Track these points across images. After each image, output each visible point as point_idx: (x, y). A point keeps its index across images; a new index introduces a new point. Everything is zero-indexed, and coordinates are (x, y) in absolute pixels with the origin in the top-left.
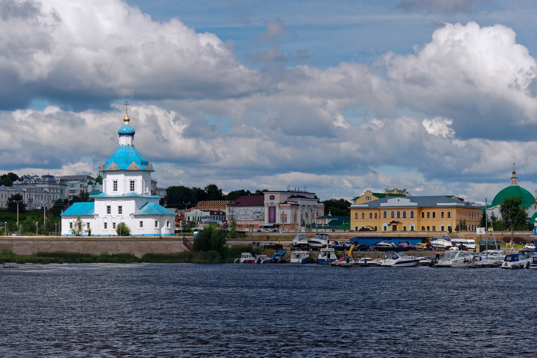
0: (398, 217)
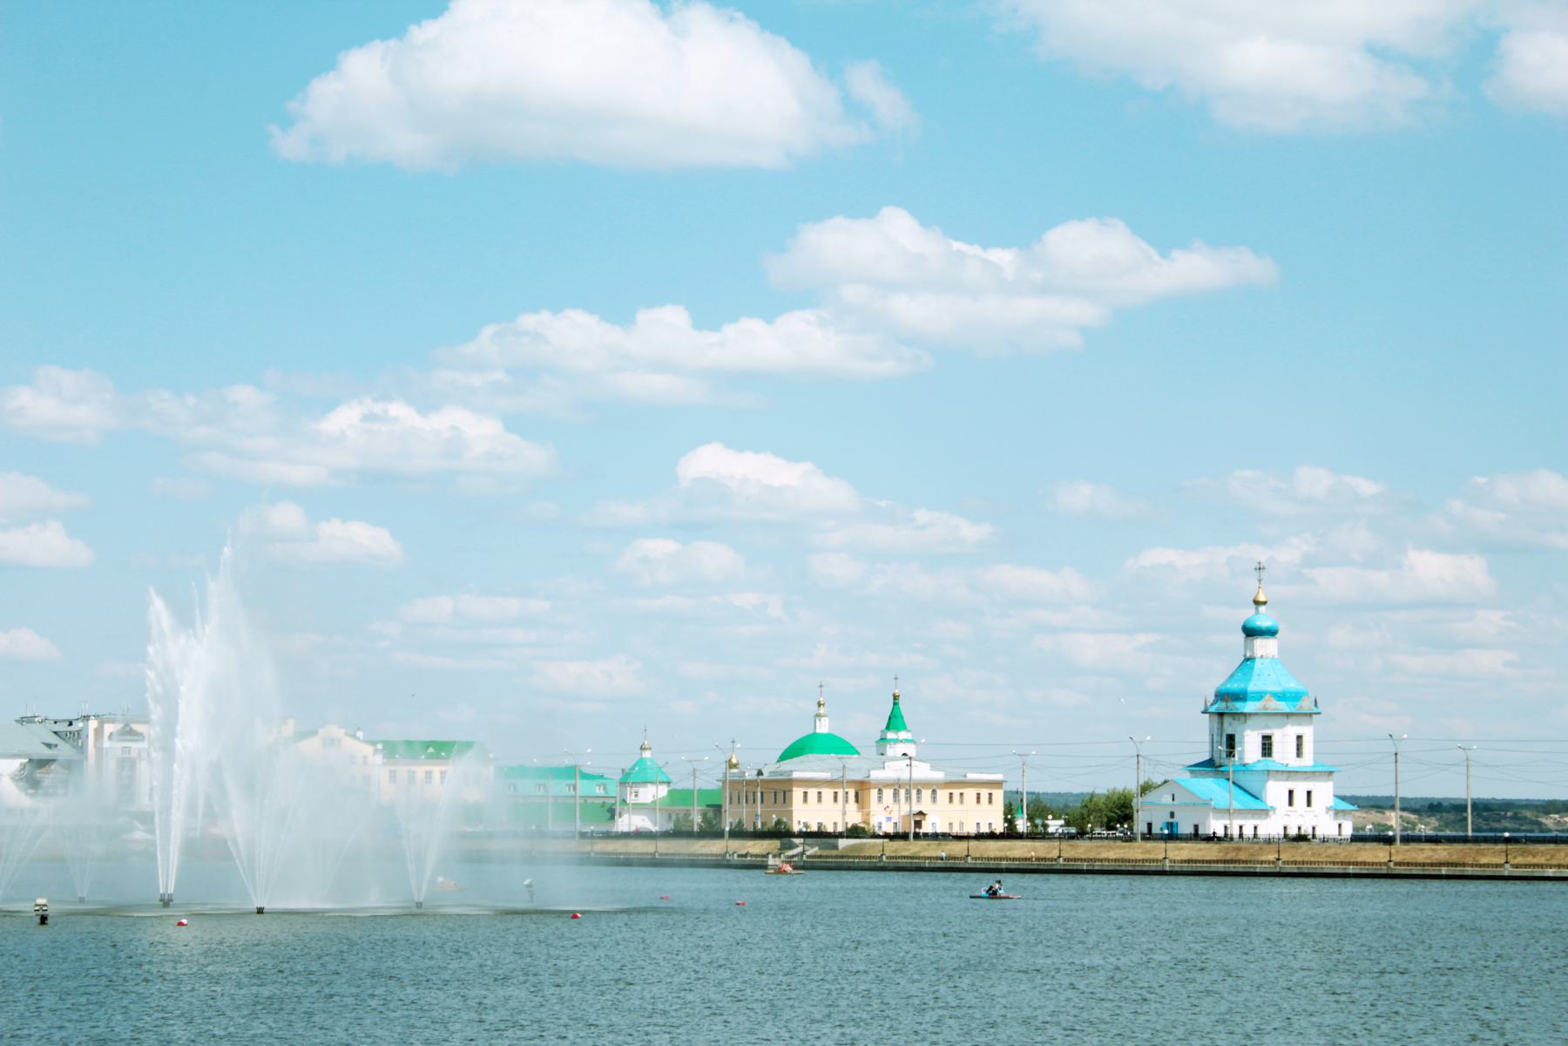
0: (909, 798)
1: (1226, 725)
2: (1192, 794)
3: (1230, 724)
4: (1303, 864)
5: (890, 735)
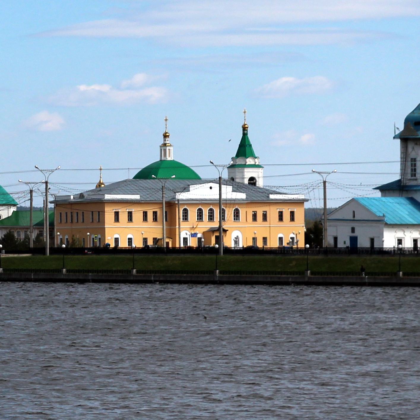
1: (410, 149)
2: (368, 210)
3: (413, 148)
4: (328, 275)
5: (240, 161)
